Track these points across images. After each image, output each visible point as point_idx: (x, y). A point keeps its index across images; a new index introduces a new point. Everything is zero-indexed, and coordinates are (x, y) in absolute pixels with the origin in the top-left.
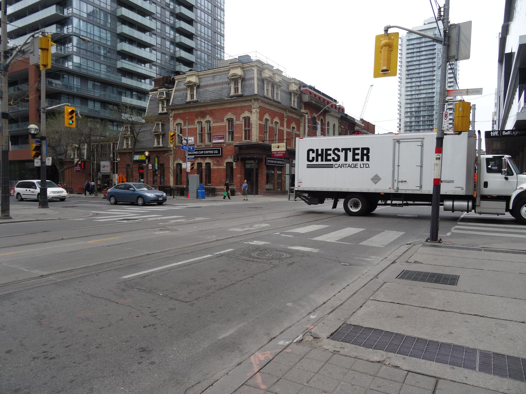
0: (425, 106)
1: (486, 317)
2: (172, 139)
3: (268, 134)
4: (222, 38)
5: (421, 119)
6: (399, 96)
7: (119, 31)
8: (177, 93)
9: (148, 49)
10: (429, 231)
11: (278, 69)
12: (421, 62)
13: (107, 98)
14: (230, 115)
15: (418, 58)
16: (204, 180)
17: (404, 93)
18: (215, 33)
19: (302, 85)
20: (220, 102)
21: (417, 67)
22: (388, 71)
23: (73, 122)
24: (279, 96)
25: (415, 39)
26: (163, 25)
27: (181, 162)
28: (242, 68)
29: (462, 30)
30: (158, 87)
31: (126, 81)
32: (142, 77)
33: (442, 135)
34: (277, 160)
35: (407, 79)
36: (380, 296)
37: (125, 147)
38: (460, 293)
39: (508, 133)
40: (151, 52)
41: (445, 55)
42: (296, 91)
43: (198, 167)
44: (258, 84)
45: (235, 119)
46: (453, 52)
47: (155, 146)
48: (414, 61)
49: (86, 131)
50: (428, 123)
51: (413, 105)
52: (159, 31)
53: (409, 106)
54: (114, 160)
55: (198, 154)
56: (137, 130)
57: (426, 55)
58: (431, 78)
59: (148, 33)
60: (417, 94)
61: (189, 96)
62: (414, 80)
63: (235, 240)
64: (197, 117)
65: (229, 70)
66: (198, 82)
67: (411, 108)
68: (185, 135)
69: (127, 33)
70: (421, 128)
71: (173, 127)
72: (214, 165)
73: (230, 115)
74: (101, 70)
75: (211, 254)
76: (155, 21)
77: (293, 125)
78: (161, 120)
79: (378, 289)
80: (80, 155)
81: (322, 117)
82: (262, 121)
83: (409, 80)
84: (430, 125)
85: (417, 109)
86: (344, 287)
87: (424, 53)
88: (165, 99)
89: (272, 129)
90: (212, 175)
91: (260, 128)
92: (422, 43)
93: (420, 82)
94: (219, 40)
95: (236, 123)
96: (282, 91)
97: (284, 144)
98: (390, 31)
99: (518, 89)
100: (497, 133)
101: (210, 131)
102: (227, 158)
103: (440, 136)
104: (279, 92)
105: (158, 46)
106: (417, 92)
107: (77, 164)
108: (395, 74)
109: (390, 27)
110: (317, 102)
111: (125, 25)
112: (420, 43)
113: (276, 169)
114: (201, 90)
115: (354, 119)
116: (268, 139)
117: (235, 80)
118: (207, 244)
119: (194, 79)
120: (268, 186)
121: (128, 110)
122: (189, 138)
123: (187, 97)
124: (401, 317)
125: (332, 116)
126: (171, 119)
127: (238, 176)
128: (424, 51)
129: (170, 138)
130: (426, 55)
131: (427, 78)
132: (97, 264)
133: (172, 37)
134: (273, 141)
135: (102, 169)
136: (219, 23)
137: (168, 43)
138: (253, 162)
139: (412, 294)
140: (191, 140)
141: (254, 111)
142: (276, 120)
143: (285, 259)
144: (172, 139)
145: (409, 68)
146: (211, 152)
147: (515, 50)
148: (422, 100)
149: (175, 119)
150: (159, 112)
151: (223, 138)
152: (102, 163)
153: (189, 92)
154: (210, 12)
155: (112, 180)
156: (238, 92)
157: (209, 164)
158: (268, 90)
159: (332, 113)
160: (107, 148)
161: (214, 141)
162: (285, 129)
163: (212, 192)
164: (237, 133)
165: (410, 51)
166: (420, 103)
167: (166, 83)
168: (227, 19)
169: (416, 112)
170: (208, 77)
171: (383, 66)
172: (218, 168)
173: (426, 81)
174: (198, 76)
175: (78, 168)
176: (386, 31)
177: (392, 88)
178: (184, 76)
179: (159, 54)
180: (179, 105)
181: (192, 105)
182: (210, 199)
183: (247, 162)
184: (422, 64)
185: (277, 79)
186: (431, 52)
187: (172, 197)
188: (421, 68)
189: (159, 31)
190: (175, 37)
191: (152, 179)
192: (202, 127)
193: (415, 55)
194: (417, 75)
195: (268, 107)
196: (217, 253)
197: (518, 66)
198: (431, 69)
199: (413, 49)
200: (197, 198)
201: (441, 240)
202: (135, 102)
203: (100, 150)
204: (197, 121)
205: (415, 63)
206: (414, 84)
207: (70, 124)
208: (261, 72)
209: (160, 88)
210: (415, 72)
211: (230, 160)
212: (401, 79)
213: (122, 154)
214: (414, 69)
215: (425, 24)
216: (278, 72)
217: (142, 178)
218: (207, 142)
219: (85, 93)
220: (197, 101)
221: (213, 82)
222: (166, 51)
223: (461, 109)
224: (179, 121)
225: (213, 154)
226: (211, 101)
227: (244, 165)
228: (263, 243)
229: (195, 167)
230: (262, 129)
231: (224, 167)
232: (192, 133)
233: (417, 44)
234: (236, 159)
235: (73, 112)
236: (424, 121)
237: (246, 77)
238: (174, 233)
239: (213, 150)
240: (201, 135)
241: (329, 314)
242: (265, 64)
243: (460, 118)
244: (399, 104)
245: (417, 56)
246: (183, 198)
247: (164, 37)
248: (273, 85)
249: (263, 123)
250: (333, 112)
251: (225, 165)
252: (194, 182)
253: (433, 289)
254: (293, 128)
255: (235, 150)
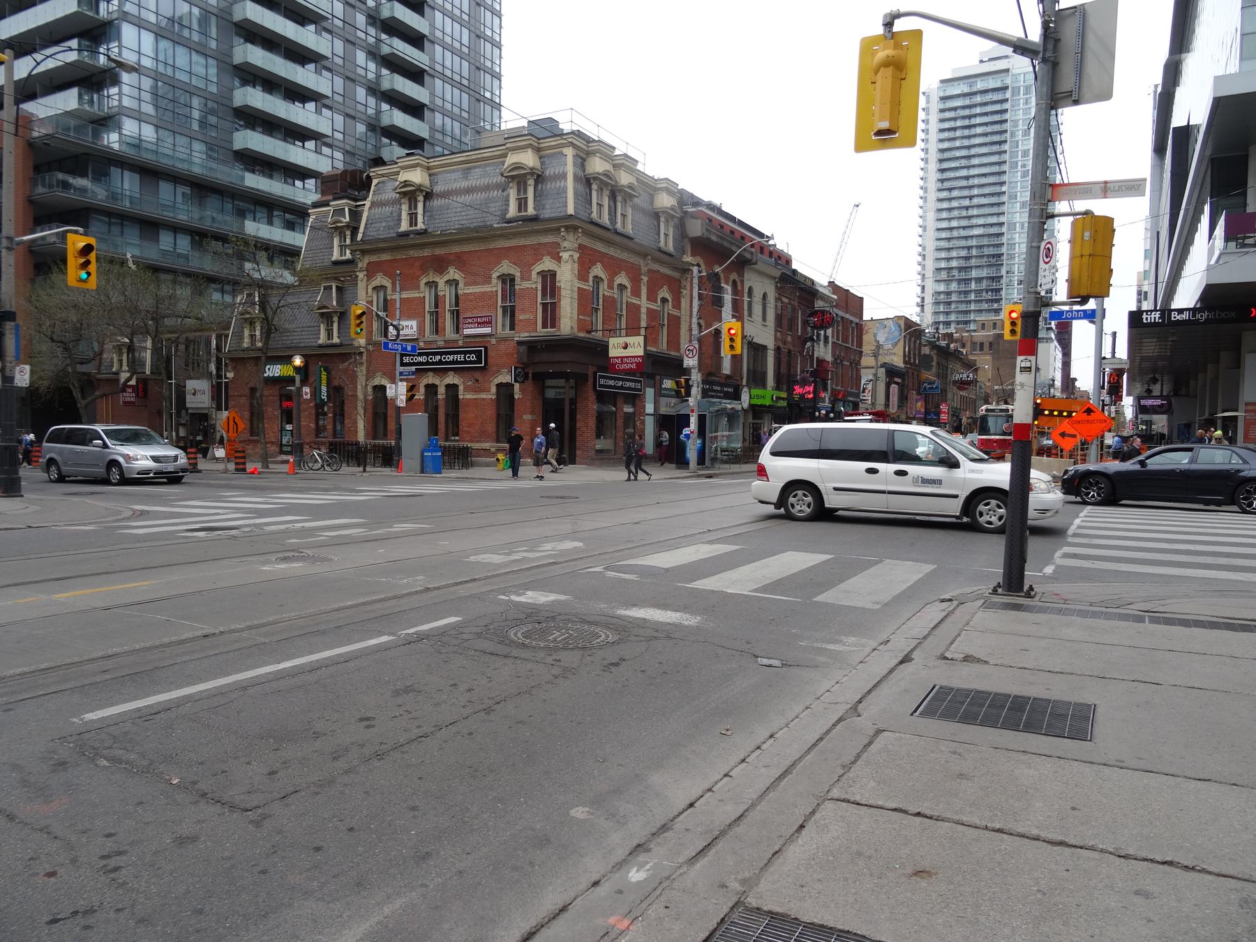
0: (982, 257)
1: (1203, 871)
2: (358, 325)
3: (600, 314)
4: (496, 82)
5: (973, 286)
6: (920, 231)
7: (238, 59)
8: (377, 211)
9: (311, 106)
10: (1001, 560)
11: (626, 155)
12: (973, 151)
13: (207, 225)
14: (506, 267)
15: (966, 142)
16: (442, 426)
17: (932, 224)
18: (478, 69)
19: (686, 199)
20: (481, 234)
21: (964, 162)
22: (894, 133)
23: (89, 274)
24: (629, 222)
25: (958, 96)
26: (349, 46)
27: (384, 382)
28: (538, 150)
29: (1092, 21)
30: (330, 197)
31: (255, 181)
32: (296, 173)
33: (1036, 305)
34: (623, 380)
35: (940, 190)
36: (864, 785)
37: (246, 343)
38: (1106, 770)
39: (1185, 316)
40: (318, 112)
41: (1045, 89)
42: (672, 208)
43: (426, 394)
44: (574, 189)
45: (518, 274)
46: (1067, 81)
47: (321, 342)
48: (957, 148)
49: (146, 303)
50: (989, 296)
51: (954, 254)
52: (339, 61)
53: (943, 255)
54: (219, 376)
55: (427, 363)
56: (273, 301)
57: (985, 135)
58: (997, 189)
59: (311, 67)
60: (964, 228)
61: (404, 216)
62: (955, 193)
63: (474, 588)
64: (424, 270)
65: (505, 156)
66: (427, 182)
67: (948, 259)
68: (393, 318)
69: (259, 63)
70: (973, 307)
71: (363, 296)
72: (466, 389)
73: (506, 267)
74: (194, 158)
75: (390, 634)
76: (329, 37)
77: (664, 293)
78: (337, 279)
79: (858, 756)
80: (135, 365)
81: (734, 276)
82: (587, 281)
83: (945, 194)
84: (992, 301)
85: (963, 263)
86: (758, 742)
87: (979, 130)
88: (348, 226)
89: (610, 303)
90: (462, 415)
91: (580, 298)
92: (975, 106)
93: (971, 198)
94: (488, 86)
95: (520, 285)
96: (634, 208)
97: (641, 339)
98: (899, 26)
99: (1207, 208)
100: (1158, 315)
101: (457, 305)
102: (498, 372)
103: (1031, 309)
104: (629, 212)
105: (337, 98)
106: (964, 223)
107: (125, 385)
108: (911, 143)
109: (898, 15)
110: (722, 238)
111: (253, 43)
112: (970, 107)
113: (620, 401)
114: (436, 203)
115: (813, 282)
116: (600, 327)
117: (519, 178)
118: (394, 602)
119: (417, 177)
120: (600, 444)
121: (262, 256)
122: (404, 323)
123: (400, 220)
124: (929, 874)
125: (760, 273)
126: (361, 275)
127: (525, 420)
128: (980, 125)
129: (353, 322)
130: (985, 135)
131: (987, 190)
132: (33, 668)
133: (371, 76)
134: (613, 332)
135: (189, 398)
136: (488, 46)
137: (361, 93)
138: (561, 382)
139: (961, 776)
140: (410, 327)
141: (565, 255)
142: (622, 279)
143: (600, 647)
144: (358, 325)
145: (946, 165)
146: (460, 358)
147: (1200, 117)
148: (974, 242)
149: (370, 276)
150: (334, 258)
151: (490, 322)
152: (191, 385)
153: (405, 207)
154: (465, 17)
155: (214, 427)
156: (526, 210)
157: (455, 386)
158: (600, 205)
159: (759, 266)
160: (202, 346)
161: (467, 332)
162: (644, 303)
163: (460, 458)
164: (523, 311)
165: (947, 125)
166: (969, 248)
167: (351, 186)
168: (508, 38)
169: (960, 269)
170: (454, 171)
171: (881, 120)
172: (478, 397)
173: (984, 195)
174: (428, 168)
175: (129, 396)
176: (889, 25)
177: (904, 173)
178: (394, 168)
179: (339, 119)
180: (384, 240)
181: (413, 240)
182: (454, 474)
183: (549, 382)
184: (974, 156)
185: (624, 179)
186: (997, 128)
187: (361, 469)
188: (974, 166)
189: (339, 61)
190: (379, 76)
191: (313, 426)
192: (436, 296)
193: (958, 133)
194: (964, 183)
195: (600, 247)
196: (411, 631)
197: (1208, 152)
198: (995, 169)
199: (955, 119)
200: (422, 472)
201: (1031, 588)
202: (276, 234)
203: (179, 353)
204: (424, 281)
205: (958, 153)
206: (955, 204)
207: (81, 280)
208: (584, 160)
209: (335, 199)
210: (958, 174)
211: (506, 378)
212: (926, 191)
213: (238, 361)
214: (956, 169)
215: (981, 61)
216: (627, 163)
217: (289, 422)
218: (449, 333)
219: (149, 210)
220: (425, 232)
221: (464, 184)
222: (355, 110)
223: (1087, 234)
224: (380, 280)
225: (465, 362)
226: (461, 231)
227: (542, 390)
228: (552, 597)
229: (420, 395)
230: (586, 301)
231: (491, 394)
232: (413, 308)
233: (964, 107)
234: (522, 376)
235: (88, 249)
236: (978, 292)
237: (547, 173)
238: (317, 569)
239: (465, 353)
240: (436, 316)
241: (693, 860)
242: (594, 141)
243: (1085, 259)
244: (920, 249)
245: (963, 138)
246: (387, 471)
247: (352, 76)
248: (615, 193)
249: (588, 286)
250: (763, 263)
251: (494, 389)
252: (415, 428)
253: (1022, 757)
254: (664, 300)
255: (518, 353)
